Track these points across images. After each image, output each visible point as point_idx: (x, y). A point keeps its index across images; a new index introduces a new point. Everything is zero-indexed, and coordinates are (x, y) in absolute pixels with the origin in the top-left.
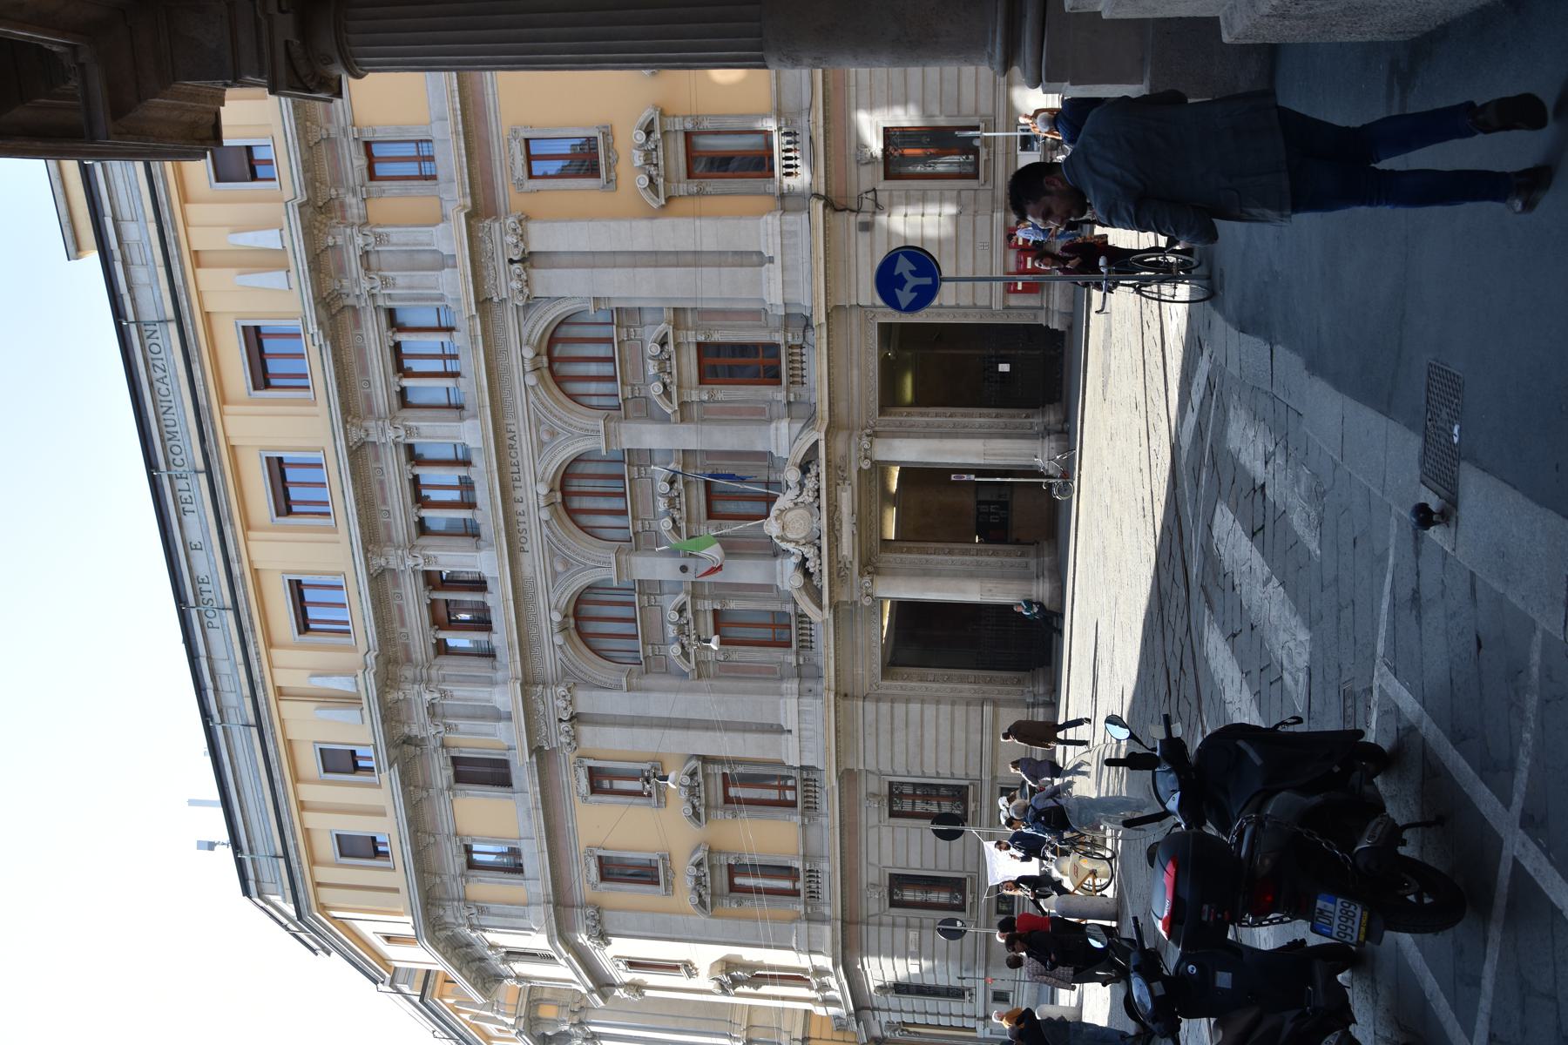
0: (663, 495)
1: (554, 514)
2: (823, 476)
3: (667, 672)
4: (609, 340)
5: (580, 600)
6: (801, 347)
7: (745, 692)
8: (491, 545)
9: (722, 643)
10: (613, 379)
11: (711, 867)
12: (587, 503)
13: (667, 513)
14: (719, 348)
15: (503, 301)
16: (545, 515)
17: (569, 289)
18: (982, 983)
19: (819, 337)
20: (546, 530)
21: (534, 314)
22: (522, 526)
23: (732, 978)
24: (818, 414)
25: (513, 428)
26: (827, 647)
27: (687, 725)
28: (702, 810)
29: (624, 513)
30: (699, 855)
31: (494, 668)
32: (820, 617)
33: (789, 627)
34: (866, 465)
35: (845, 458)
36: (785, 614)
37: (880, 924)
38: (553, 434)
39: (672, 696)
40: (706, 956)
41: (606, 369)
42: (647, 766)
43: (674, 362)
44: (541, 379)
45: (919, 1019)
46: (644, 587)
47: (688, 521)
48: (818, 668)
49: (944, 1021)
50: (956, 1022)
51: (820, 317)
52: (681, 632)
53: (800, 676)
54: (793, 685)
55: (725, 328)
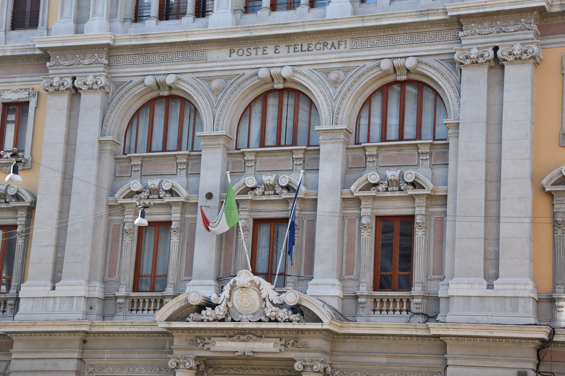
0: (277, 180)
1: (264, 82)
2: (289, 326)
3: (116, 177)
4: (419, 136)
5: (185, 101)
6: (408, 311)
7: (93, 248)
8: (237, 23)
9: (141, 229)
10: (384, 138)
12: (272, 112)
13: (261, 183)
14: (409, 236)
15: (459, 40)
16: (263, 73)
17: (468, 100)
19: (416, 328)
20: (249, 73)
21: (445, 69)
22: (253, 52)
24: (346, 324)
25: (342, 47)
26: (132, 325)
27: (66, 193)
28: (249, 197)
29: (262, 144)
31: (125, 20)
32: (160, 319)
33: (152, 290)
34: (298, 366)
35: (305, 348)
36: (164, 286)
38: (335, 83)
39: (93, 180)
41: (392, 133)
42: (27, 155)
43: (397, 194)
44: (386, 74)
46: (194, 160)
47: (253, 202)
48: (112, 316)
51: (435, 329)
52: (152, 191)
53: (105, 299)
54: (97, 291)
55: (427, 241)
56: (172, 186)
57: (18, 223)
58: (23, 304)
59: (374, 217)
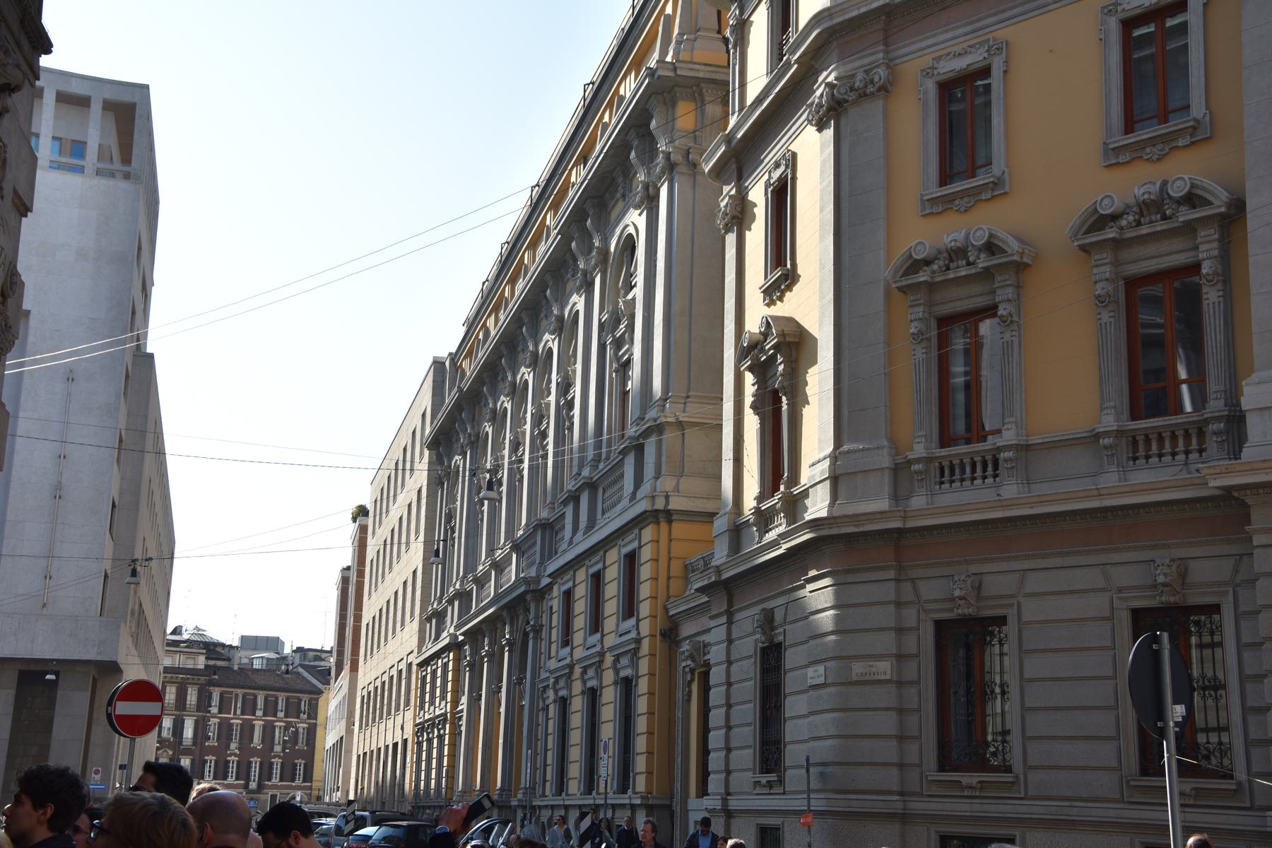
11: (988, 274)
18: (798, 803)
23: (772, 359)
28: (1110, 233)
30: (1013, 245)
37: (899, 604)
40: (811, 305)
45: (716, 696)
49: (716, 739)
50: (716, 760)
56: (1193, 186)
57: (1201, 256)
58: (1255, 427)
59: (1121, 283)
